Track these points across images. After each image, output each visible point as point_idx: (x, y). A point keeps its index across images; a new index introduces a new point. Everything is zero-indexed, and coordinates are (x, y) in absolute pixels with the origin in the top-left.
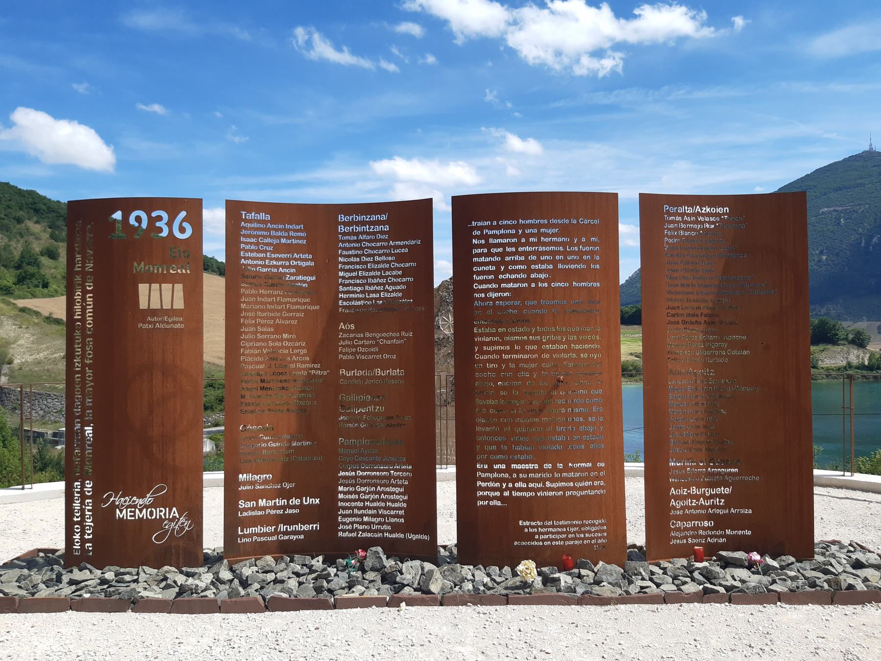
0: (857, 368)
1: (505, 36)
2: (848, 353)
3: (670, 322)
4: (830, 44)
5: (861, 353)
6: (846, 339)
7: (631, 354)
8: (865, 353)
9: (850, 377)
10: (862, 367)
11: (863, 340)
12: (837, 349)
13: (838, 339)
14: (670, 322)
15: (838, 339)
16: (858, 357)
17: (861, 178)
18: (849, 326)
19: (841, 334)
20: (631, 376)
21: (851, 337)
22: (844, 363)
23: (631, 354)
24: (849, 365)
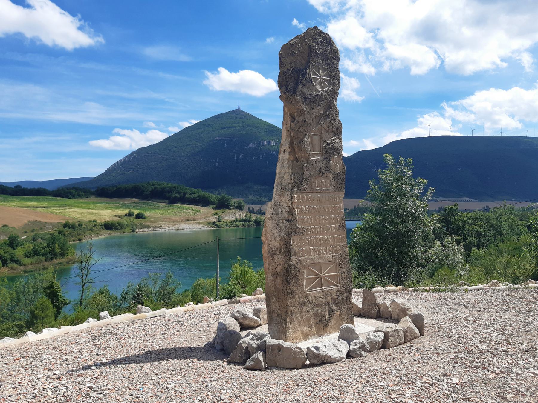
0: (240, 221)
1: (331, 18)
2: (235, 213)
3: (32, 271)
4: (155, 52)
5: (241, 213)
6: (234, 206)
7: (116, 216)
8: (243, 213)
9: (237, 226)
10: (242, 220)
11: (242, 207)
12: (230, 211)
13: (231, 206)
14: (32, 271)
15: (231, 206)
16: (240, 215)
17: (235, 123)
18: (234, 201)
19: (232, 203)
20: (117, 229)
21: (236, 205)
22: (234, 219)
23: (116, 216)
24: (236, 220)
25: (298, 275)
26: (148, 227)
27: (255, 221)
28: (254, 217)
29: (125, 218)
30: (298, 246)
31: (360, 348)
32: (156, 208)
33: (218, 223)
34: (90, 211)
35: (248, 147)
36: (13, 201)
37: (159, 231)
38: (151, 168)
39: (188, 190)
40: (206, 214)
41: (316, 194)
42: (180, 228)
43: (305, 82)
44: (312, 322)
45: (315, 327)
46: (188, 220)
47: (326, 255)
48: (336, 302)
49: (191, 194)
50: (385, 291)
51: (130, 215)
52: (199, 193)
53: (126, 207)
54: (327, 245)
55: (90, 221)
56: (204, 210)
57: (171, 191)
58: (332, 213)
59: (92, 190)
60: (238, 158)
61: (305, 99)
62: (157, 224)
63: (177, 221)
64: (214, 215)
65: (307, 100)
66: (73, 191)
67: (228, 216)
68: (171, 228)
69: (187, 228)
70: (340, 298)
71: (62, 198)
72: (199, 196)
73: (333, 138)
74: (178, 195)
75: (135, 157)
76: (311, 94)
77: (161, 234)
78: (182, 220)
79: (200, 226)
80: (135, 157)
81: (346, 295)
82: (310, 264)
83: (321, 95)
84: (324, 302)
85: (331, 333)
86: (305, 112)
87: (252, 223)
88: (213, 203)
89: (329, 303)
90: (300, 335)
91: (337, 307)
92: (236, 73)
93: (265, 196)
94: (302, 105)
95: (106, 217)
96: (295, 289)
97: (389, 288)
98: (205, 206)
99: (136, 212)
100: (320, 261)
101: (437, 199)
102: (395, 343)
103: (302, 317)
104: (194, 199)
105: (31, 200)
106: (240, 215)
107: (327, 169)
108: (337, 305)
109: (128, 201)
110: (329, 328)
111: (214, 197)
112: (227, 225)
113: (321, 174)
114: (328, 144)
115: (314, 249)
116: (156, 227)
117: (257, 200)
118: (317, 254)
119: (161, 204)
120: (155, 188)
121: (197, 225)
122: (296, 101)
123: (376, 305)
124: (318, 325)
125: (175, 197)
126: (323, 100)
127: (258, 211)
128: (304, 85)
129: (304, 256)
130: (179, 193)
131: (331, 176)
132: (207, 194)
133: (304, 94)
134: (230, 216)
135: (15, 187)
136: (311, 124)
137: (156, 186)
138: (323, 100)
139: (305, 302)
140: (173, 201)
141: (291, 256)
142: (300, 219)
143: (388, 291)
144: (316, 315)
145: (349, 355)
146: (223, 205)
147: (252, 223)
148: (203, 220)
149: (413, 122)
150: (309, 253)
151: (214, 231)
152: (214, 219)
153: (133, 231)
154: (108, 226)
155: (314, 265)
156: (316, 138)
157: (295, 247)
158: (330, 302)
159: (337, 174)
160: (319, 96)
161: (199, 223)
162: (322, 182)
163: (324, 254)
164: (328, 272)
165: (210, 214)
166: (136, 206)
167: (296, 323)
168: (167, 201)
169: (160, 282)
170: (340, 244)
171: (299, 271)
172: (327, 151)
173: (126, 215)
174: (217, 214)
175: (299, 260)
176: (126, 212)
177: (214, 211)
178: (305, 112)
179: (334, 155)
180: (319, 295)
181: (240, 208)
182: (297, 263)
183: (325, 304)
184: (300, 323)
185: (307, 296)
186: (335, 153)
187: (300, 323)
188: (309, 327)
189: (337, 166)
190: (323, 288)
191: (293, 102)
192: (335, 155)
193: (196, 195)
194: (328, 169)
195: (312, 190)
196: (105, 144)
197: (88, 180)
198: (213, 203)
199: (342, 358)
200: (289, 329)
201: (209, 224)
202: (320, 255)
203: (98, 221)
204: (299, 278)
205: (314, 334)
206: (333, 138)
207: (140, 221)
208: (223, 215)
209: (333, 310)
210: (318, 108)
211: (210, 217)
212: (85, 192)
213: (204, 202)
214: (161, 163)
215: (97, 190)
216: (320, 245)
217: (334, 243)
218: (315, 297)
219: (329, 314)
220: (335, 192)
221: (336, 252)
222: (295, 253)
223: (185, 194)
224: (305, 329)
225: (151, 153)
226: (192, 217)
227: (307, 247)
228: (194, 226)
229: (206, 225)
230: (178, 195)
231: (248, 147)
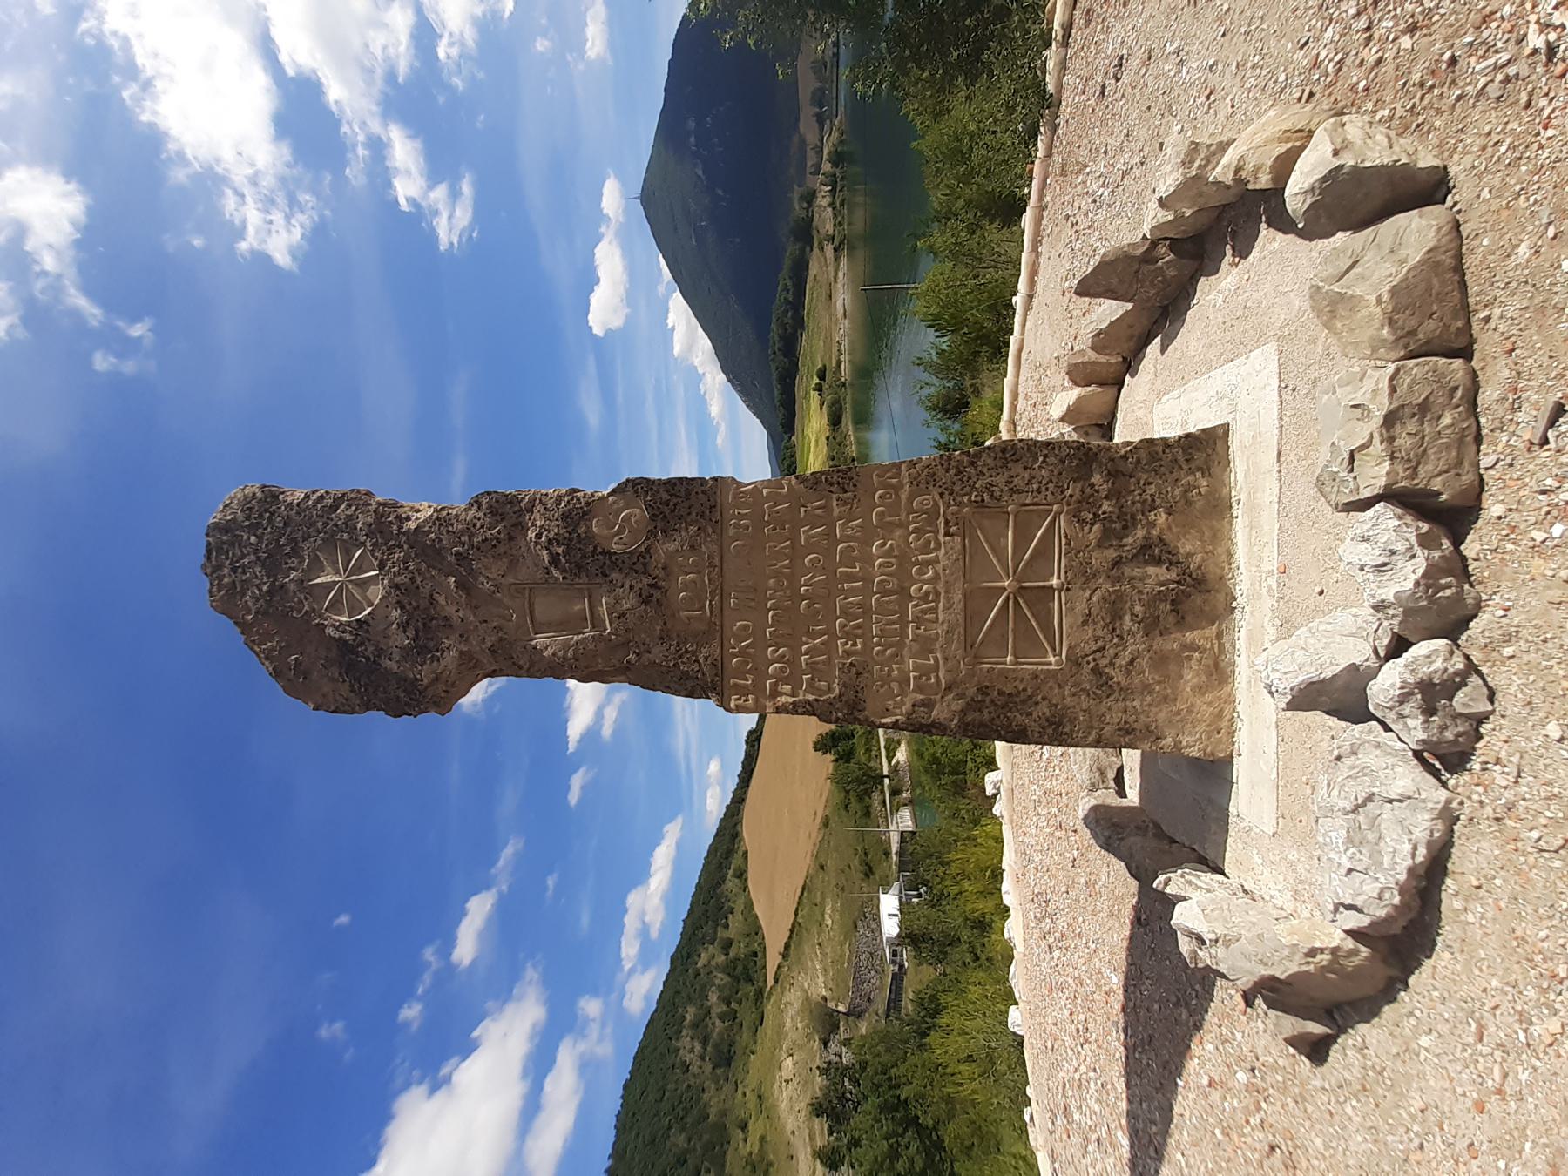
9: (842, 204)
10: (833, 192)
18: (798, 208)
24: (831, 204)
25: (1001, 693)
26: (839, 363)
27: (835, 164)
28: (827, 167)
30: (903, 693)
31: (1429, 711)
37: (845, 346)
39: (780, 297)
40: (821, 263)
41: (726, 613)
43: (371, 649)
44: (1171, 644)
45: (1192, 629)
47: (939, 567)
48: (1117, 526)
50: (1065, 43)
51: (819, 388)
52: (785, 278)
53: (807, 393)
54: (904, 559)
56: (814, 269)
57: (783, 326)
58: (794, 538)
61: (422, 650)
62: (835, 350)
65: (424, 647)
66: (786, 463)
67: (824, 222)
69: (843, 298)
70: (1106, 506)
73: (531, 534)
76: (404, 627)
77: (851, 343)
79: (840, 274)
81: (1097, 479)
82: (968, 644)
83: (397, 587)
84: (1107, 586)
85: (1230, 555)
86: (461, 653)
87: (838, 171)
88: (803, 251)
89: (1117, 563)
90: (1209, 697)
91: (1135, 526)
94: (443, 663)
96: (1044, 708)
97: (1056, 26)
99: (816, 380)
100: (958, 597)
102: (1461, 441)
103: (1147, 688)
104: (794, 285)
106: (823, 200)
107: (639, 567)
108: (1128, 523)
109: (799, 393)
110: (1212, 570)
111: (792, 249)
112: (840, 224)
113: (657, 594)
114: (555, 560)
115: (919, 621)
118: (934, 610)
122: (437, 679)
123: (1149, 257)
124: (1189, 618)
126: (412, 580)
128: (380, 652)
129: (936, 669)
131: (665, 548)
133: (406, 653)
134: (825, 221)
136: (498, 629)
138: (412, 580)
139: (1096, 671)
140: (800, 323)
141: (933, 724)
142: (811, 687)
143: (1068, 28)
144: (1151, 626)
145: (1446, 759)
146: (805, 233)
147: (838, 171)
148: (831, 269)
150: (925, 646)
151: (851, 248)
152: (829, 248)
153: (844, 384)
154: (835, 421)
155: (972, 617)
156: (545, 607)
157: (902, 703)
158: (1112, 554)
159: (653, 517)
160: (402, 593)
161: (835, 278)
162: (685, 588)
163: (937, 576)
164: (1002, 560)
167: (1162, 716)
169: (926, 377)
170: (904, 497)
171: (984, 690)
172: (579, 567)
174: (820, 243)
175: (949, 688)
176: (814, 394)
177: (816, 250)
178: (461, 653)
179: (589, 537)
180: (1081, 607)
181: (810, 197)
182: (959, 697)
183: (1119, 580)
184: (1165, 698)
185: (1075, 661)
186: (582, 530)
187: (1165, 698)
188: (1189, 658)
189: (627, 519)
190: (1055, 582)
191: (441, 686)
192: (589, 528)
193: (789, 283)
194: (638, 562)
195: (714, 630)
196: (715, 409)
198: (803, 251)
199: (1449, 817)
200: (1177, 743)
201: (837, 259)
202: (937, 594)
204: (1008, 689)
205: (1219, 636)
206: (531, 534)
208: (823, 232)
209: (1146, 547)
210: (441, 599)
213: (801, 268)
216: (903, 592)
217: (900, 525)
218: (1085, 623)
219: (1158, 562)
220: (720, 526)
221: (932, 516)
222: (923, 704)
223: (787, 301)
224: (1191, 676)
226: (824, 293)
227: (906, 652)
228: (839, 285)
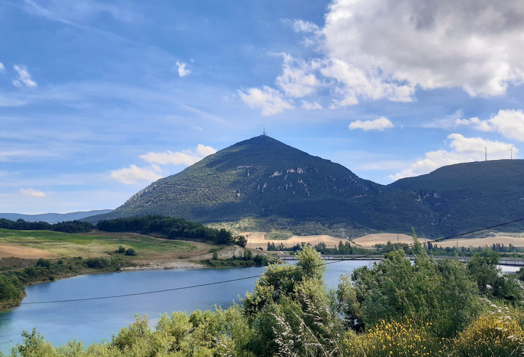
7: (106, 252)
20: (101, 267)
23: (106, 252)
29: (115, 255)
32: (152, 245)
33: (213, 262)
34: (81, 246)
35: (273, 176)
36: (11, 235)
38: (170, 200)
42: (169, 266)
46: (181, 258)
49: (190, 229)
51: (121, 251)
55: (75, 258)
56: (200, 246)
59: (94, 225)
60: (261, 188)
62: (144, 262)
63: (168, 258)
64: (211, 251)
68: (159, 267)
71: (61, 233)
72: (197, 231)
74: (176, 230)
75: (154, 188)
78: (174, 257)
80: (154, 188)
92: (475, 138)
93: (290, 230)
95: (95, 254)
98: (203, 242)
101: (495, 234)
104: (192, 234)
105: (29, 235)
109: (125, 236)
116: (143, 265)
117: (52, 249)
119: (159, 239)
120: (156, 222)
121: (189, 263)
125: (174, 231)
127: (280, 247)
130: (178, 227)
132: (226, 227)
135: (18, 220)
137: (156, 220)
149: (440, 139)
165: (207, 251)
166: (133, 242)
168: (166, 236)
173: (116, 252)
197: (108, 212)
201: (202, 262)
203: (84, 258)
207: (128, 258)
211: (205, 254)
212: (85, 226)
214: (181, 194)
215: (98, 225)
225: (171, 184)
229: (198, 263)
230: (176, 230)
231: (273, 176)
